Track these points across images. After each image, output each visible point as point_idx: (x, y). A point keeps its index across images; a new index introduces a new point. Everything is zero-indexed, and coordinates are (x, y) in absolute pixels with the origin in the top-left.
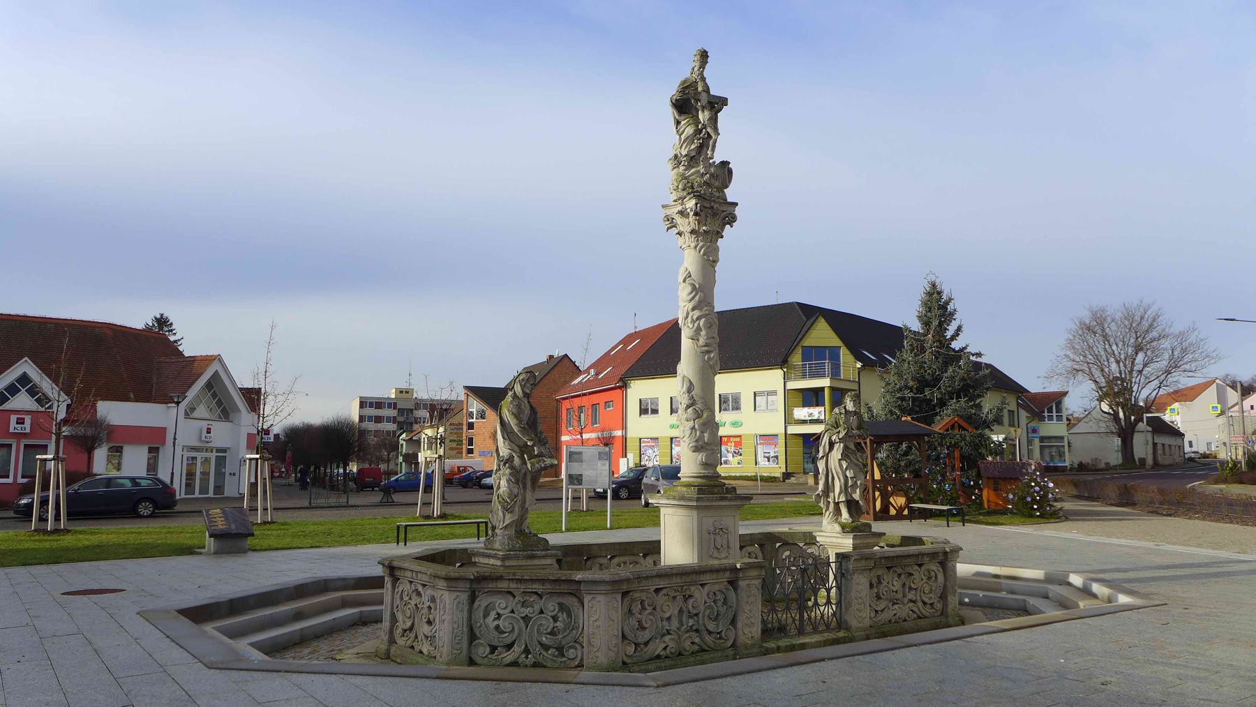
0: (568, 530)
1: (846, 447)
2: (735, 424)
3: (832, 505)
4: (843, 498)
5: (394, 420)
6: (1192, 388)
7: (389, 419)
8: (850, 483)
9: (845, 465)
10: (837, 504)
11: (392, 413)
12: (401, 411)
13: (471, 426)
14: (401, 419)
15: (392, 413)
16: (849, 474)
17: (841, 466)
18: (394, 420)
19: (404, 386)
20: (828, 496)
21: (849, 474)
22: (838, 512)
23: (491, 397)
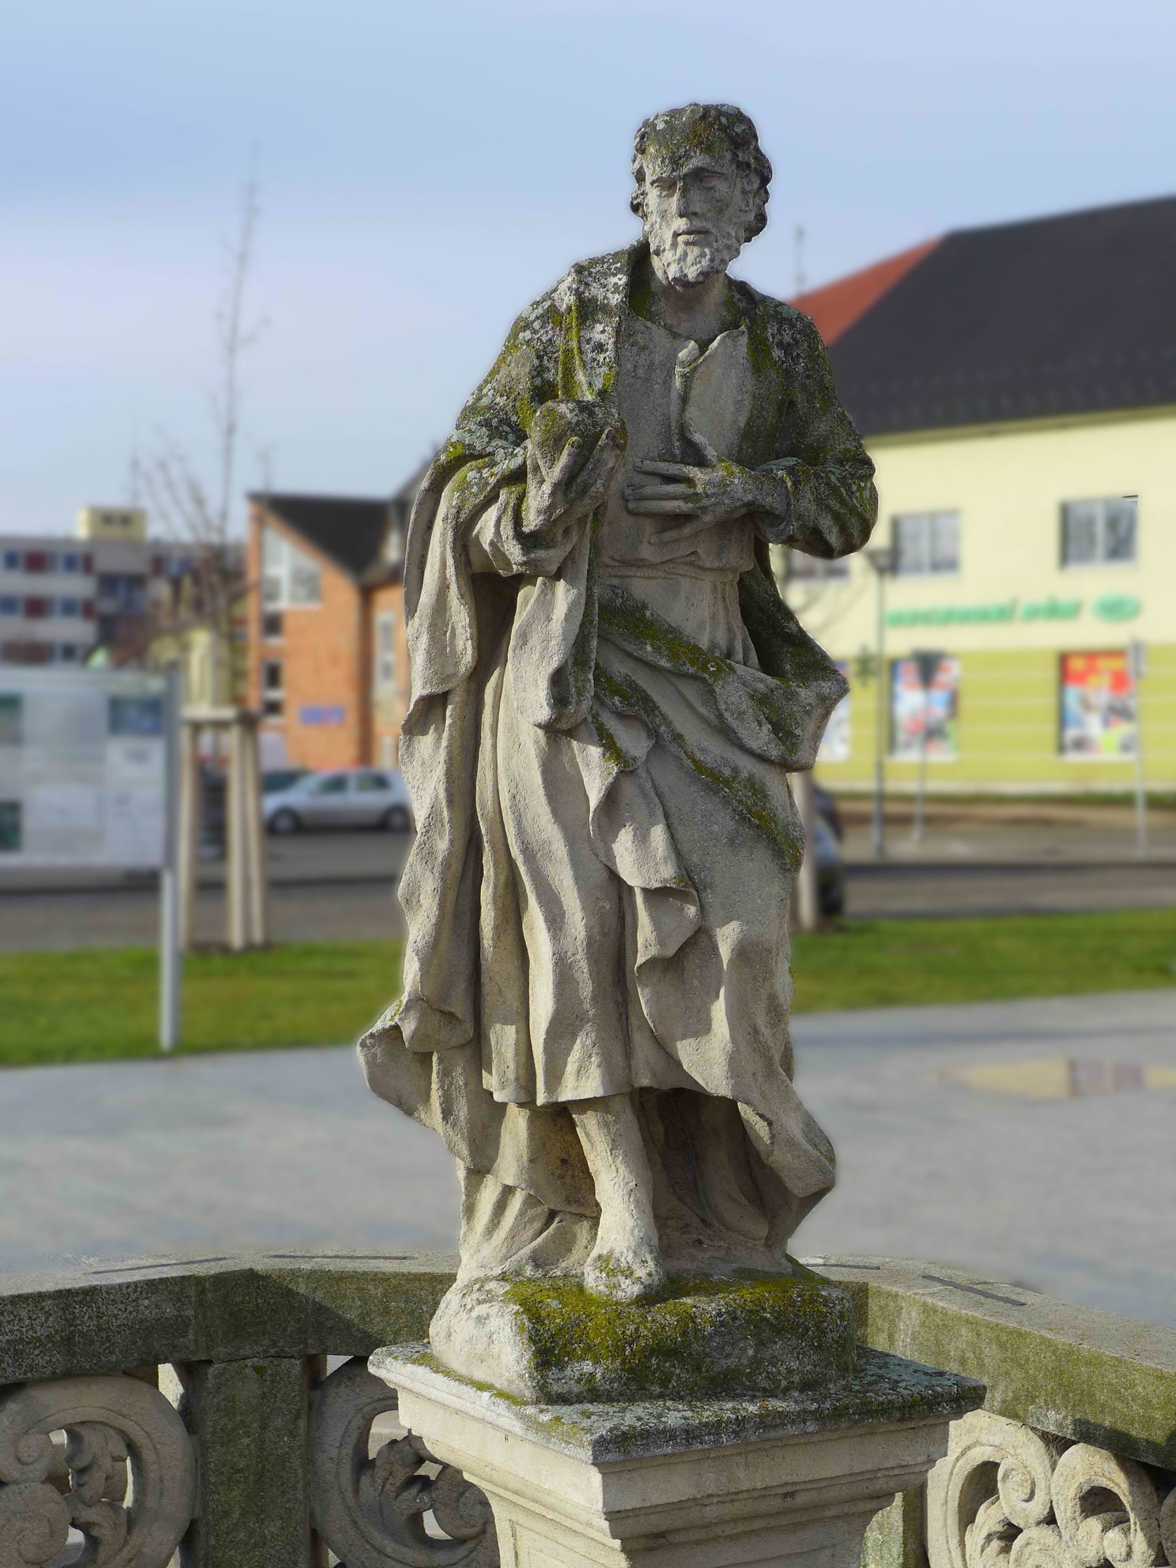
0: (189, 1047)
1: (610, 621)
2: (1115, 610)
3: (516, 1130)
4: (583, 1080)
5: (87, 609)
6: (359, 1441)
7: (70, 608)
8: (646, 940)
9: (594, 772)
10: (558, 1120)
11: (78, 586)
12: (109, 582)
13: (273, 625)
14: (108, 606)
15: (78, 586)
16: (640, 858)
17: (560, 784)
18: (87, 609)
19: (116, 499)
20: (477, 1051)
21: (640, 858)
22: (564, 1190)
23: (343, 531)
